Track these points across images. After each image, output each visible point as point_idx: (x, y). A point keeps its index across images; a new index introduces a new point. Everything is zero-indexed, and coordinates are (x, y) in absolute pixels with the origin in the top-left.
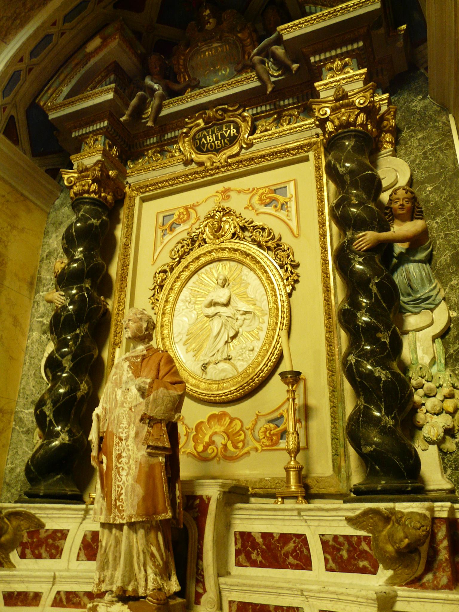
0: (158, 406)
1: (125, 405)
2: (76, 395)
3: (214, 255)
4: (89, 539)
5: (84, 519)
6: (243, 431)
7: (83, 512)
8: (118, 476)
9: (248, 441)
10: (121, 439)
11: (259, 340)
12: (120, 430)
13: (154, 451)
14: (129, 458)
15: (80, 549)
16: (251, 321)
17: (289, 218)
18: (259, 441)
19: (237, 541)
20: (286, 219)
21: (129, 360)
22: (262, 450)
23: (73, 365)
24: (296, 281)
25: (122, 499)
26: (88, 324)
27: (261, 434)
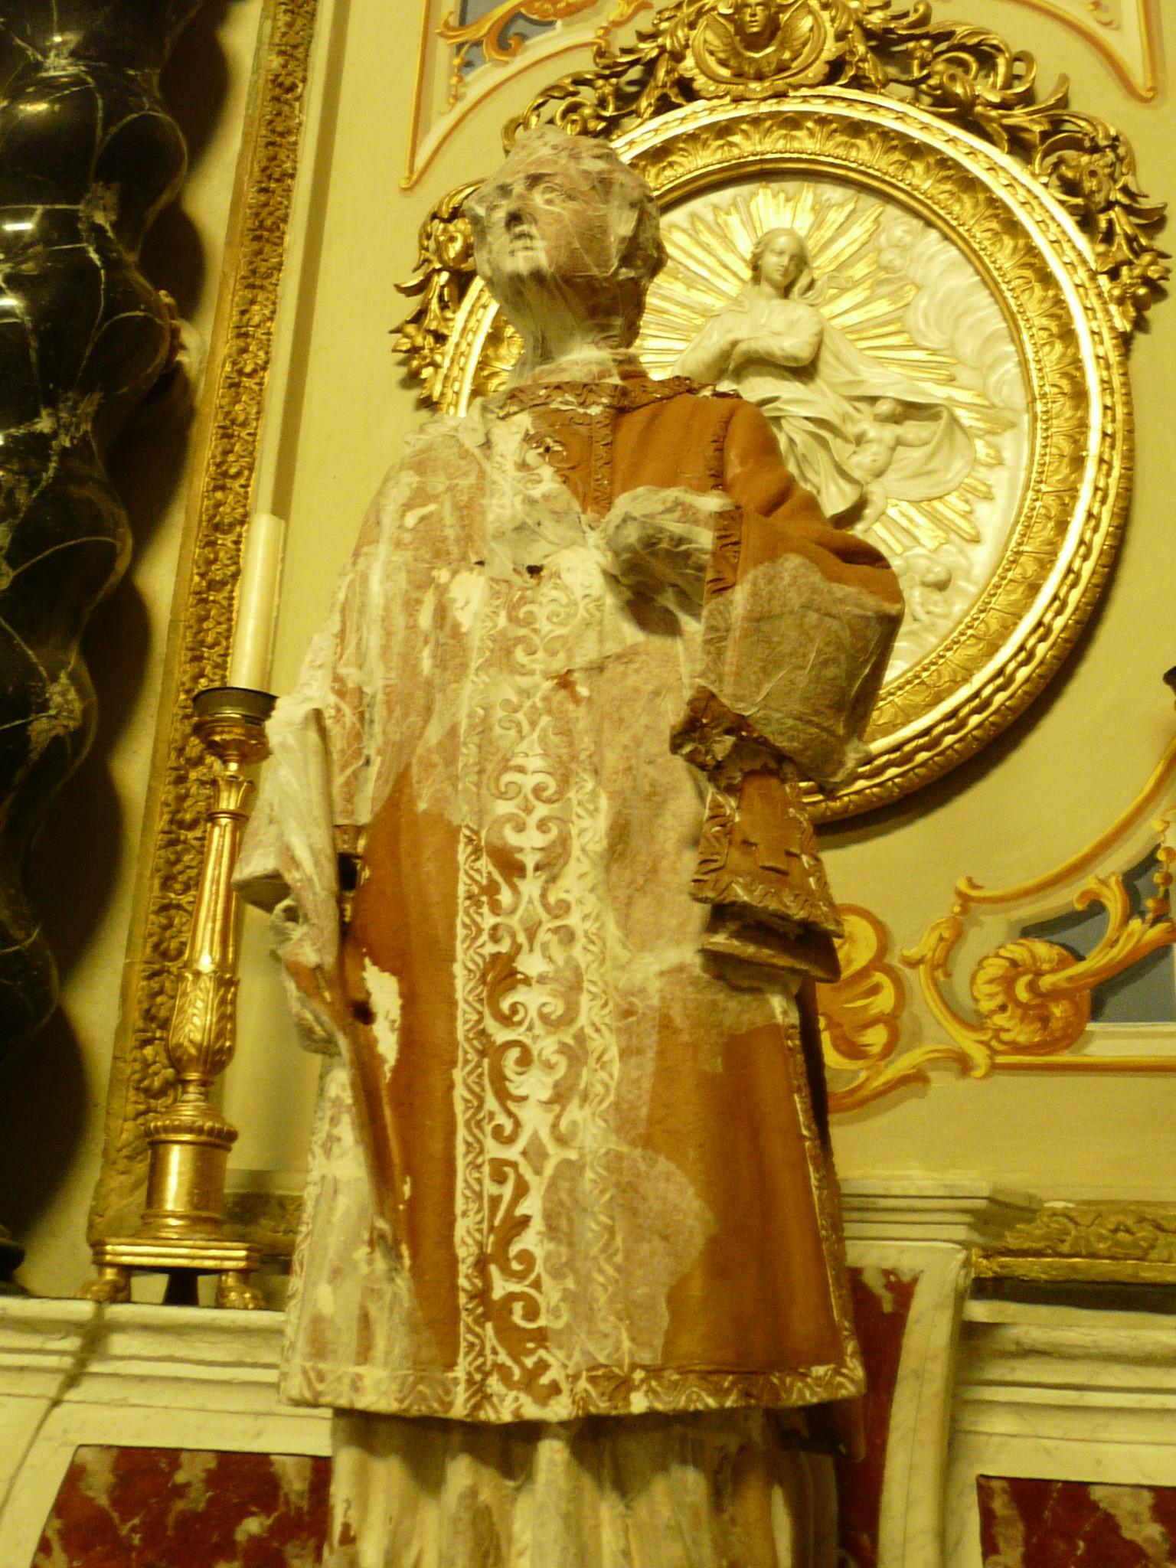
0: (778, 666)
1: (520, 655)
2: (24, 726)
3: (747, 146)
4: (99, 1488)
5: (72, 1380)
6: (889, 971)
7: (73, 1343)
8: (491, 1103)
9: (915, 1018)
10: (510, 866)
11: (976, 540)
12: (503, 808)
13: (750, 950)
14: (573, 988)
15: (44, 1547)
16: (933, 454)
17: (1106, 18)
18: (975, 1022)
19: (999, 1530)
20: (1089, 22)
21: (538, 407)
22: (994, 1068)
23: (15, 583)
24: (1157, 291)
25: (526, 1257)
26: (97, 397)
27: (983, 989)
